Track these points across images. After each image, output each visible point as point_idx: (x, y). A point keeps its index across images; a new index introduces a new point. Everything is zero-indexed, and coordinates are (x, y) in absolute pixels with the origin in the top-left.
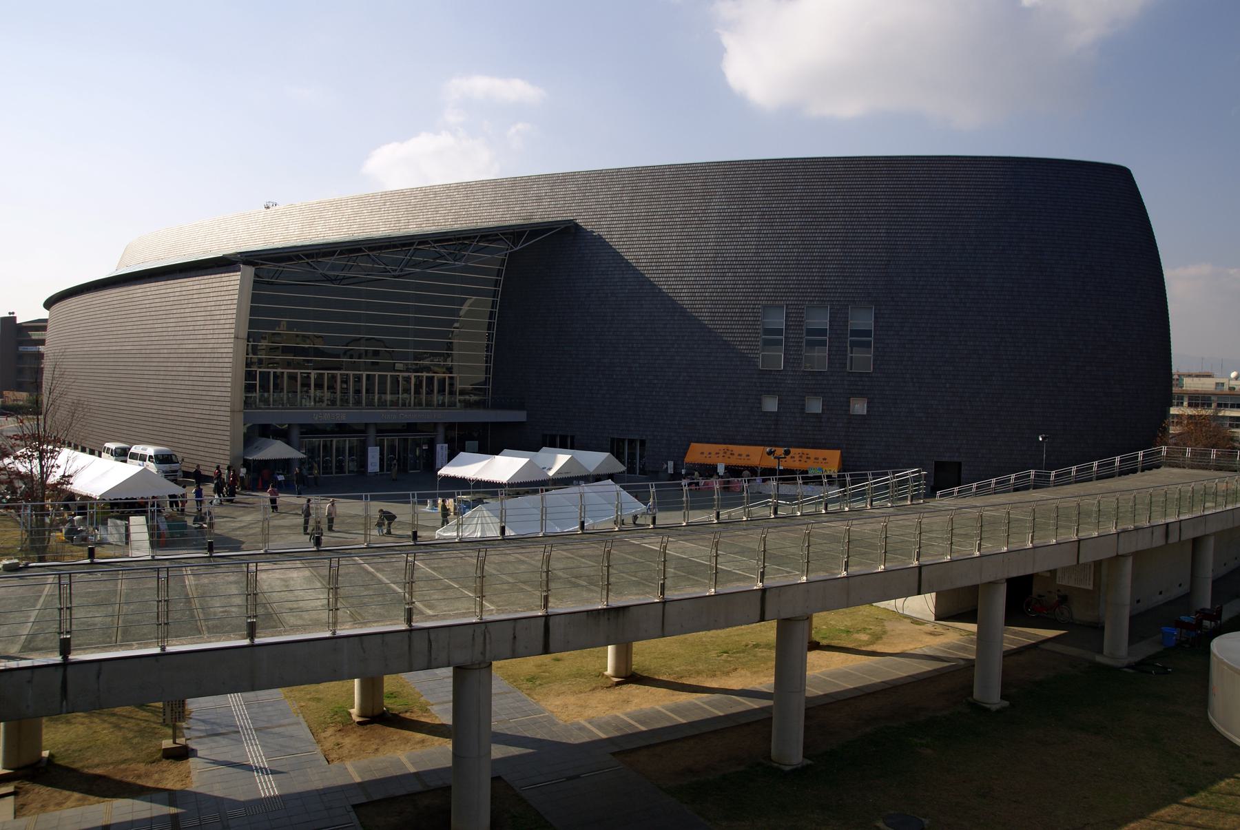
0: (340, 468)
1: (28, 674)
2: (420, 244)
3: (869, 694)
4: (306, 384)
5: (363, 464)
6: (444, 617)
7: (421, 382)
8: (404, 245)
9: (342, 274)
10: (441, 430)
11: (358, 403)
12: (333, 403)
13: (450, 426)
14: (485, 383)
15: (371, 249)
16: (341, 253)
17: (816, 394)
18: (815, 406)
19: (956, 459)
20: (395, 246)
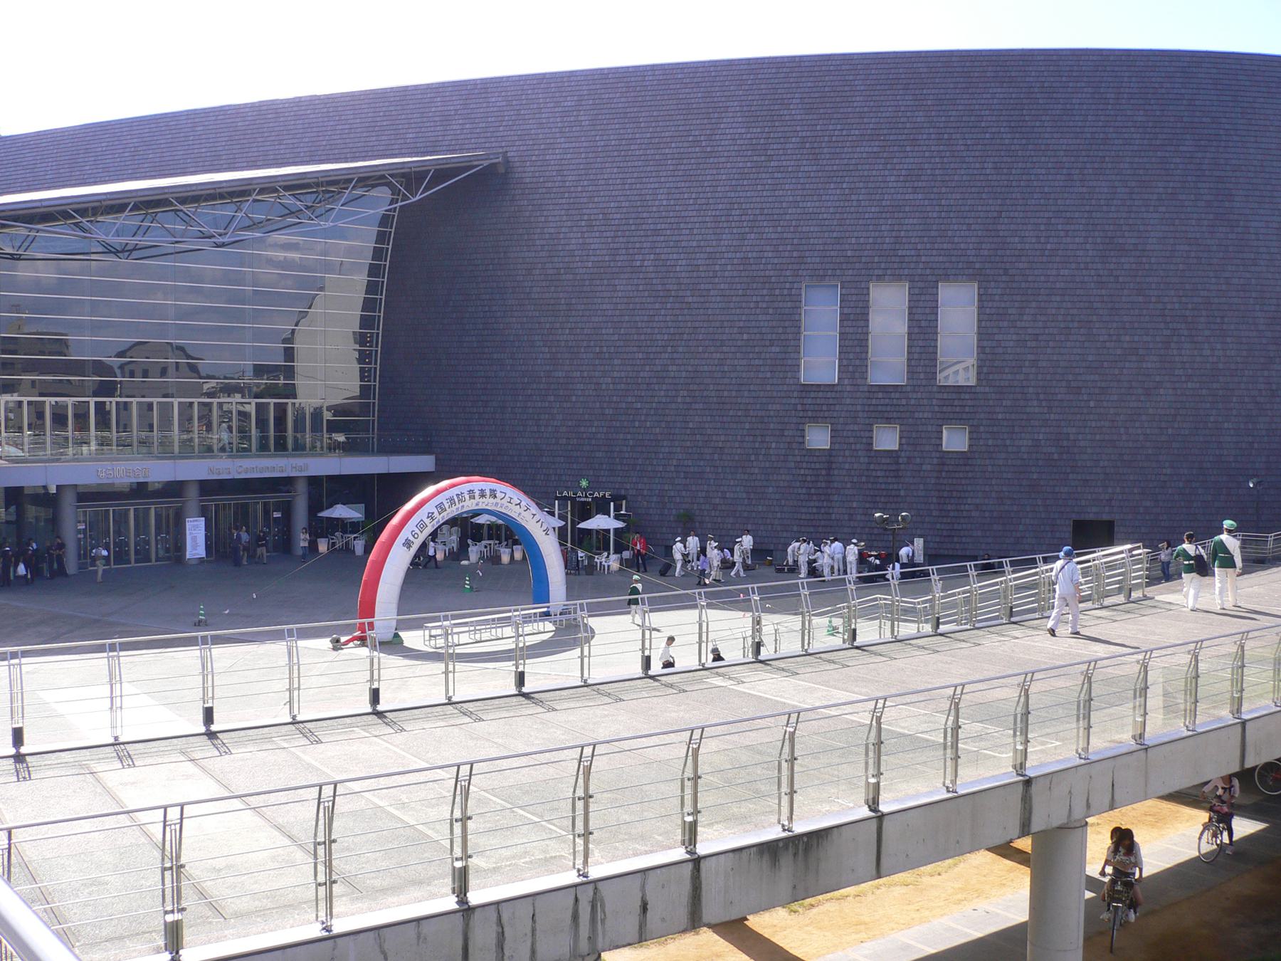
0: (143, 555)
1: (527, 906)
2: (262, 191)
3: (630, 945)
4: (81, 417)
5: (179, 546)
6: (917, 796)
7: (285, 411)
8: (231, 194)
9: (133, 241)
10: (192, 493)
11: (263, 447)
12: (186, 445)
13: (208, 488)
14: (365, 409)
15: (183, 201)
16: (136, 207)
17: (888, 420)
18: (887, 439)
19: (1105, 517)
20: (222, 196)
